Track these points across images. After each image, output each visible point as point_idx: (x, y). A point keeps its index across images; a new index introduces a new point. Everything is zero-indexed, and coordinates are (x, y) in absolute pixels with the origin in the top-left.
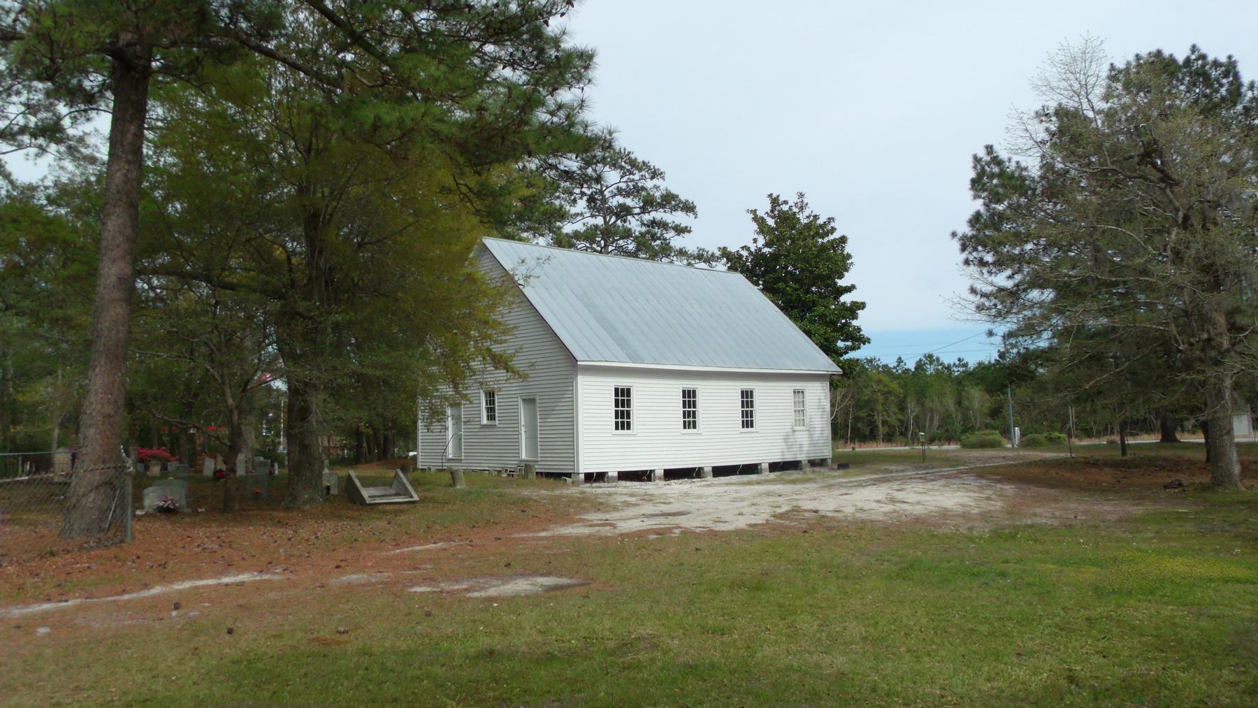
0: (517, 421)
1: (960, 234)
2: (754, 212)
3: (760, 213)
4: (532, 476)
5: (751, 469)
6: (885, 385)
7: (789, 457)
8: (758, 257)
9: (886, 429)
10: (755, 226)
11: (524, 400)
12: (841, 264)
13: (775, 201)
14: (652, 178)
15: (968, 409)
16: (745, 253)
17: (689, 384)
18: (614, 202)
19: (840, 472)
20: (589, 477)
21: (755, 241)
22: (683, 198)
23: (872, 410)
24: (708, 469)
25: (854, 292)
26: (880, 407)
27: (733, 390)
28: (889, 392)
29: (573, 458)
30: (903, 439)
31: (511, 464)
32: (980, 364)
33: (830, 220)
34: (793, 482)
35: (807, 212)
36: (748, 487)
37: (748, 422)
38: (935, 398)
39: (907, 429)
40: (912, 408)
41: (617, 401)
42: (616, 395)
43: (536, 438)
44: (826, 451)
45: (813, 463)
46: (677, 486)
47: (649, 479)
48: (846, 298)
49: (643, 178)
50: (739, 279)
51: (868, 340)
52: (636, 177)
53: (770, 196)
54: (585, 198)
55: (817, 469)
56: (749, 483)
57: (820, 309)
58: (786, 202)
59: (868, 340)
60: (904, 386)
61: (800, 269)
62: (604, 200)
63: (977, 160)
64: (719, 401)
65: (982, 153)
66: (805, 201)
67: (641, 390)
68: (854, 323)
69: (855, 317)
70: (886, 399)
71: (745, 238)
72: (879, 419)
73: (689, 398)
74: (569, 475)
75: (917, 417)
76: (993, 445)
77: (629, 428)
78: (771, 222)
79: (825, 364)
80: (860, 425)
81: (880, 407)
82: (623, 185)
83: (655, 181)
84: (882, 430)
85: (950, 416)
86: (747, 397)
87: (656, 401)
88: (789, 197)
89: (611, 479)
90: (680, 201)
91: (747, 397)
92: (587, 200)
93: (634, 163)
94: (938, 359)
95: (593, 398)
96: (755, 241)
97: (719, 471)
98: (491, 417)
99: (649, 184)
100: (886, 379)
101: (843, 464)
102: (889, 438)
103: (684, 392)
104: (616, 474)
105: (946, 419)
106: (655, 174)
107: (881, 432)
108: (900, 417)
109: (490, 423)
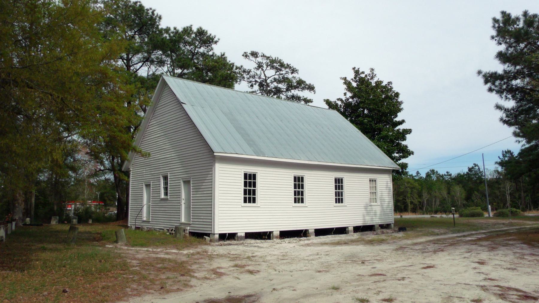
0: (179, 196)
1: (483, 74)
3: (349, 79)
5: (342, 231)
6: (411, 184)
7: (369, 223)
8: (347, 105)
9: (412, 206)
10: (345, 86)
12: (396, 108)
13: (357, 72)
14: (292, 73)
15: (454, 196)
16: (339, 103)
17: (299, 173)
18: (272, 86)
19: (401, 234)
20: (223, 237)
21: (345, 94)
22: (308, 83)
23: (405, 196)
24: (312, 231)
25: (404, 124)
26: (409, 195)
27: (330, 177)
28: (414, 188)
29: (211, 223)
30: (421, 211)
32: (458, 174)
33: (390, 83)
34: (371, 242)
35: (375, 79)
36: (339, 248)
37: (339, 199)
38: (436, 190)
39: (423, 206)
40: (425, 196)
43: (190, 208)
44: (391, 217)
45: (382, 226)
46: (289, 244)
48: (401, 127)
49: (287, 73)
50: (335, 114)
51: (413, 153)
52: (284, 72)
53: (354, 69)
54: (257, 84)
55: (384, 230)
56: (339, 243)
57: (384, 133)
58: (363, 73)
59: (413, 153)
60: (421, 185)
61: (372, 110)
62: (268, 85)
63: (495, 20)
64: (319, 185)
65: (499, 17)
66: (375, 73)
67: (264, 176)
68: (404, 143)
69: (404, 139)
70: (412, 191)
71: (339, 93)
72: (408, 201)
73: (299, 182)
74: (208, 235)
75: (427, 200)
76: (480, 215)
77: (342, 202)
78: (354, 84)
79: (387, 163)
80: (399, 204)
81: (409, 195)
82: (277, 77)
83: (293, 75)
84: (410, 206)
85: (445, 200)
86: (339, 183)
87: (274, 184)
90: (307, 85)
91: (339, 183)
92: (259, 85)
93: (282, 65)
94: (437, 172)
95: (227, 181)
96: (345, 94)
97: (319, 232)
98: (166, 194)
99: (290, 76)
100: (412, 181)
101: (402, 227)
102: (414, 211)
103: (295, 178)
104: (243, 235)
105: (443, 201)
106: (294, 71)
107: (410, 207)
108: (419, 200)
109: (165, 197)
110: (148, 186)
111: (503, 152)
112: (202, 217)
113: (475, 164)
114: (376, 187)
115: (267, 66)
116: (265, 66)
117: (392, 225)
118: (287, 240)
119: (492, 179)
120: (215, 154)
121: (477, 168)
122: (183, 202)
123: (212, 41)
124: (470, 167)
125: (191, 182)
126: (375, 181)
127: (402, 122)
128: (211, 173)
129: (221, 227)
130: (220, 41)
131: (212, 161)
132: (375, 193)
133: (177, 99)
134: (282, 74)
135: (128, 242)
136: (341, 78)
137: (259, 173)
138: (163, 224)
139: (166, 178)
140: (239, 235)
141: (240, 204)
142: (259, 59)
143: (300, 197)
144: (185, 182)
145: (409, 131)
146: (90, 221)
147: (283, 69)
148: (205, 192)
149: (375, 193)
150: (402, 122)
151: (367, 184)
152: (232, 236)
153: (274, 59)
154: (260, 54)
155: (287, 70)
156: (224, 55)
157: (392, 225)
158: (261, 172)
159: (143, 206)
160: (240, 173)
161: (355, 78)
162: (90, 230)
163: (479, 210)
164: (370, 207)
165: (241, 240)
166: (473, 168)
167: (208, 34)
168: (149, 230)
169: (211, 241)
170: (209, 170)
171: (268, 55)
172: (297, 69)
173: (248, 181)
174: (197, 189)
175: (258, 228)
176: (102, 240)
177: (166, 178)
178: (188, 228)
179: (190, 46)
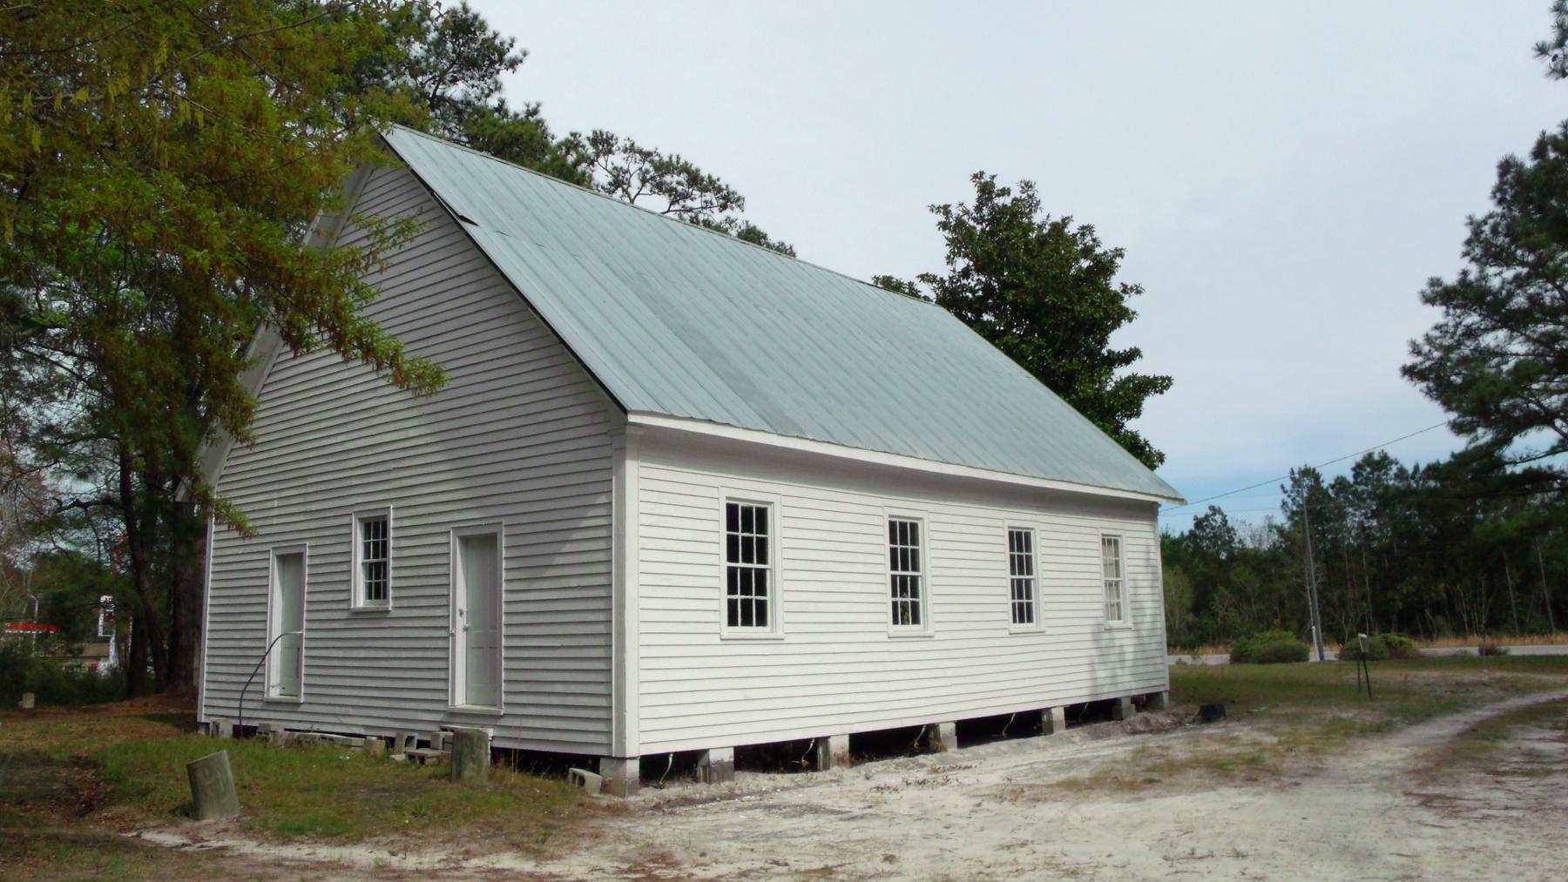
0: (263, 600)
2: (946, 210)
4: (479, 769)
5: (1027, 724)
7: (1107, 693)
11: (466, 541)
14: (723, 207)
20: (655, 768)
21: (950, 260)
24: (947, 729)
31: (425, 721)
41: (732, 541)
42: (732, 525)
43: (494, 646)
46: (886, 772)
47: (813, 766)
49: (707, 205)
52: (697, 204)
53: (977, 176)
58: (1005, 192)
67: (802, 520)
74: (592, 763)
76: (1283, 656)
77: (762, 621)
83: (728, 212)
88: (1008, 179)
89: (715, 773)
93: (694, 179)
95: (666, 525)
98: (377, 590)
101: (1207, 705)
104: (728, 756)
106: (729, 199)
109: (374, 605)
110: (292, 561)
111: (1292, 472)
112: (560, 688)
113: (1212, 508)
114: (1117, 563)
115: (644, 181)
116: (635, 182)
117: (1165, 696)
118: (875, 767)
119: (1256, 550)
120: (632, 418)
121: (1218, 518)
122: (461, 622)
123: (501, 60)
124: (1201, 516)
125: (504, 542)
126: (1116, 542)
127: (1131, 356)
128: (603, 499)
129: (647, 730)
130: (527, 60)
131: (606, 452)
132: (1117, 583)
133: (443, 206)
134: (691, 210)
135: (248, 808)
136: (932, 209)
137: (777, 506)
138: (355, 713)
139: (376, 528)
140: (713, 756)
141: (714, 628)
142: (618, 159)
143: (909, 599)
144: (284, 560)
145: (1159, 384)
146: (28, 702)
147: (696, 193)
148: (574, 582)
149: (1117, 583)
150: (1131, 356)
151: (1095, 554)
152: (687, 764)
153: (666, 159)
154: (621, 143)
155: (709, 196)
156: (535, 112)
157: (1165, 696)
158: (787, 501)
159: (263, 638)
160: (714, 504)
161: (978, 209)
162: (42, 745)
163: (1291, 641)
164: (1106, 636)
165: (721, 778)
166: (1207, 517)
167: (489, 34)
168: (299, 742)
169: (605, 788)
170: (598, 488)
171: (646, 149)
172: (740, 193)
173: (740, 534)
174: (534, 569)
175: (794, 724)
176: (111, 799)
177: (376, 528)
178: (491, 732)
179: (414, 76)
